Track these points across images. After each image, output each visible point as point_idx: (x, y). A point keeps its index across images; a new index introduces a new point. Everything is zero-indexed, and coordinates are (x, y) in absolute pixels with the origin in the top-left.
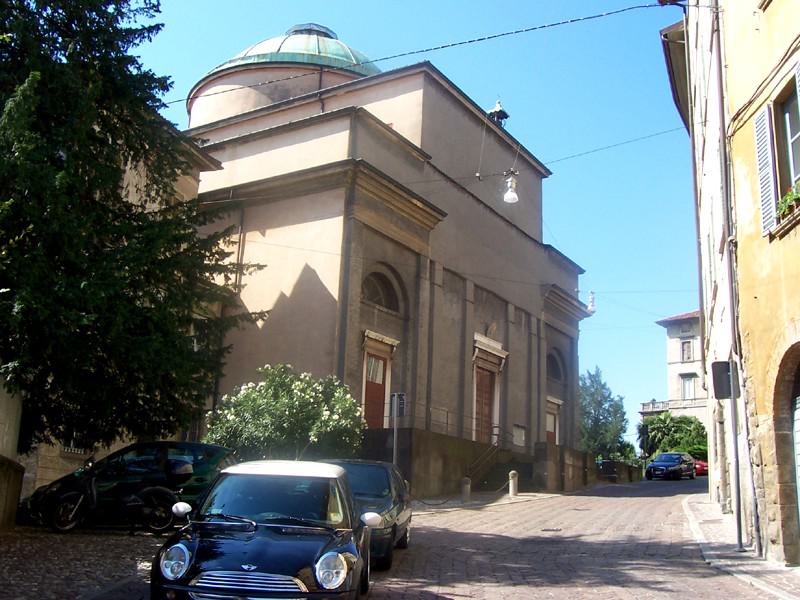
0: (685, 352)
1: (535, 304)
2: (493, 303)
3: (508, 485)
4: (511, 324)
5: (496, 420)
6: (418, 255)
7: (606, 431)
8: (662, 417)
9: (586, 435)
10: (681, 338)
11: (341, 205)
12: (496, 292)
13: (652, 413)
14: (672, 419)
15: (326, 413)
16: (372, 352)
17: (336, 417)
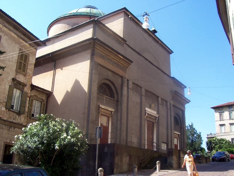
0: (221, 117)
1: (169, 98)
2: (153, 97)
3: (156, 167)
4: (160, 105)
5: (155, 140)
6: (122, 77)
7: (196, 144)
8: (214, 139)
9: (189, 146)
10: (219, 113)
11: (89, 56)
12: (154, 92)
13: (211, 138)
14: (218, 140)
15: (65, 135)
16: (102, 113)
17: (69, 137)
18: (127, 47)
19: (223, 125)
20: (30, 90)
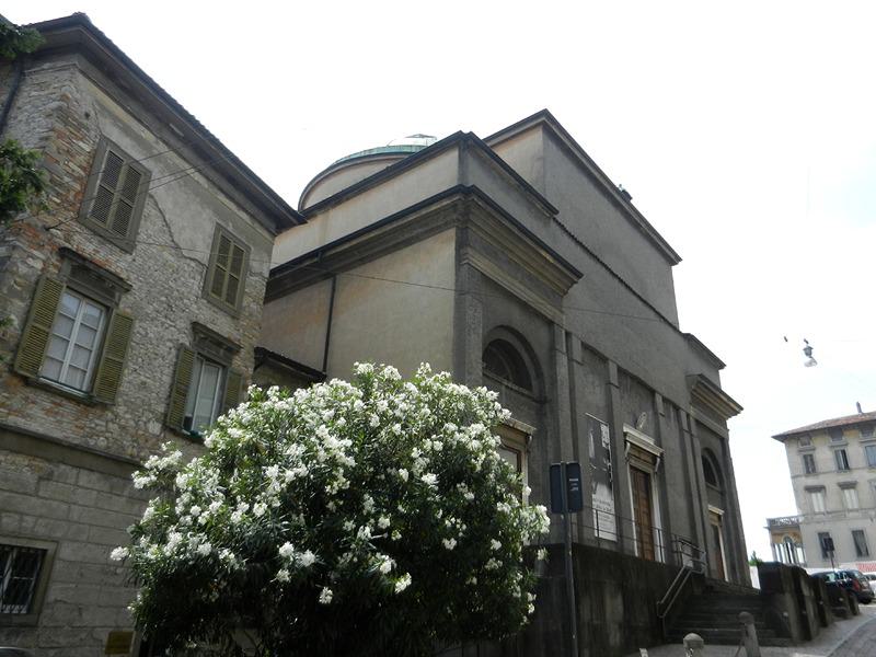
4: (661, 417)
6: (550, 323)
18: (559, 231)
19: (820, 489)
20: (253, 366)
